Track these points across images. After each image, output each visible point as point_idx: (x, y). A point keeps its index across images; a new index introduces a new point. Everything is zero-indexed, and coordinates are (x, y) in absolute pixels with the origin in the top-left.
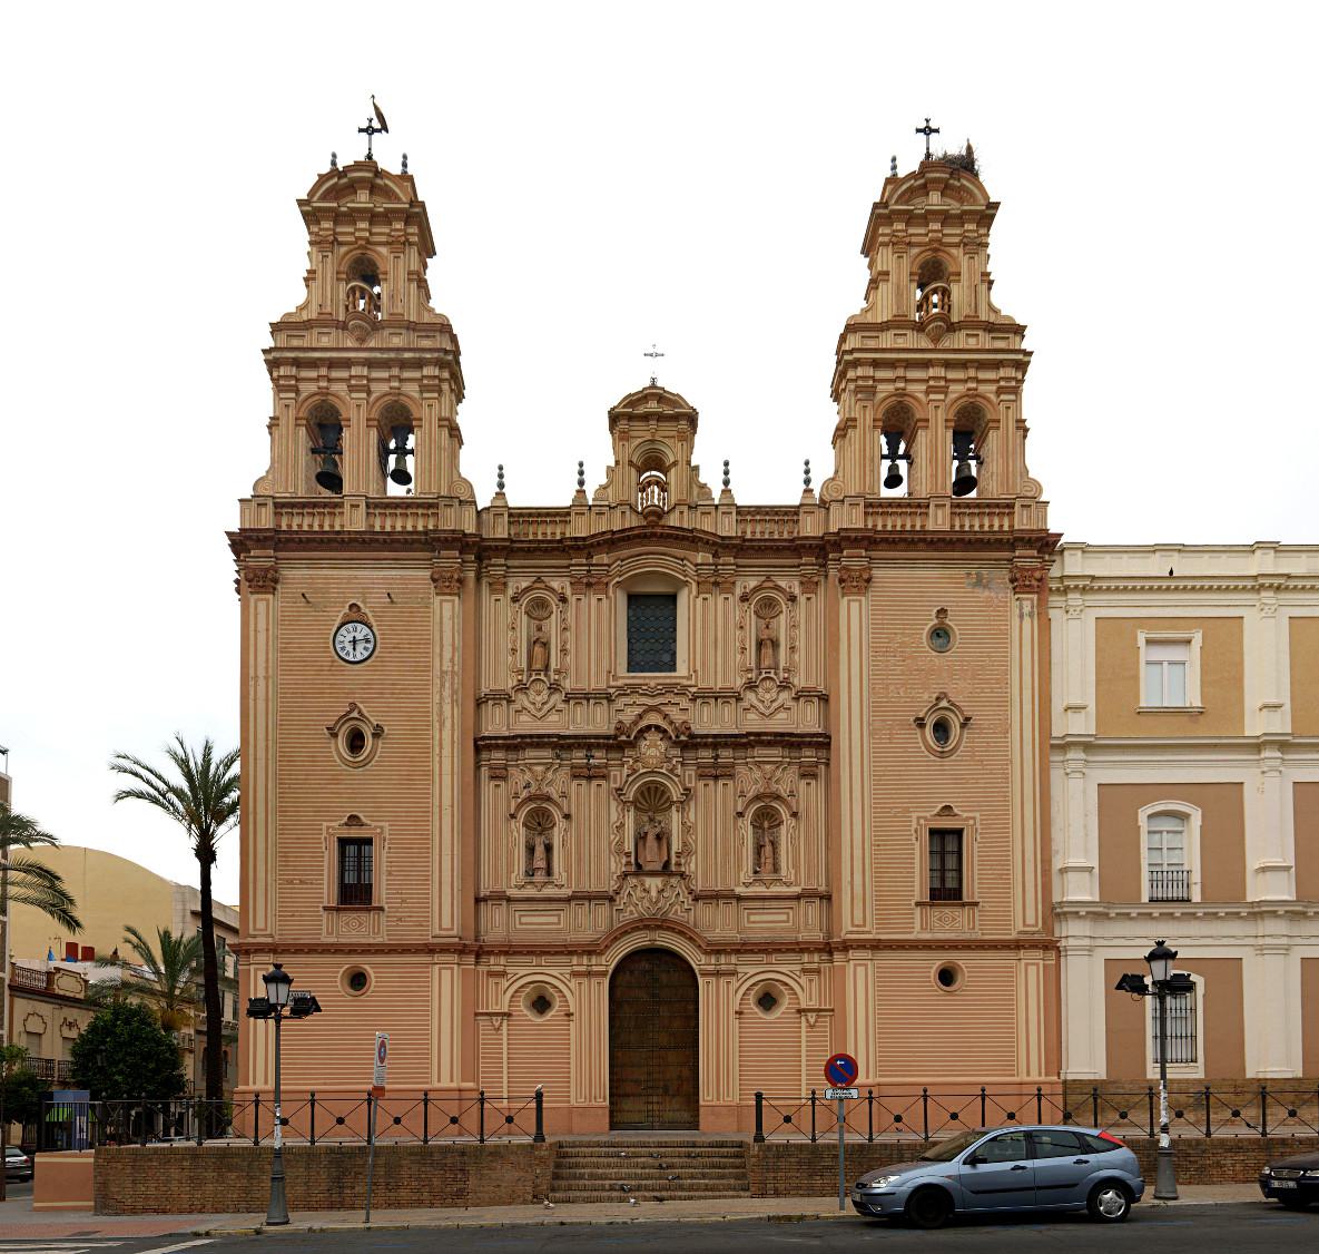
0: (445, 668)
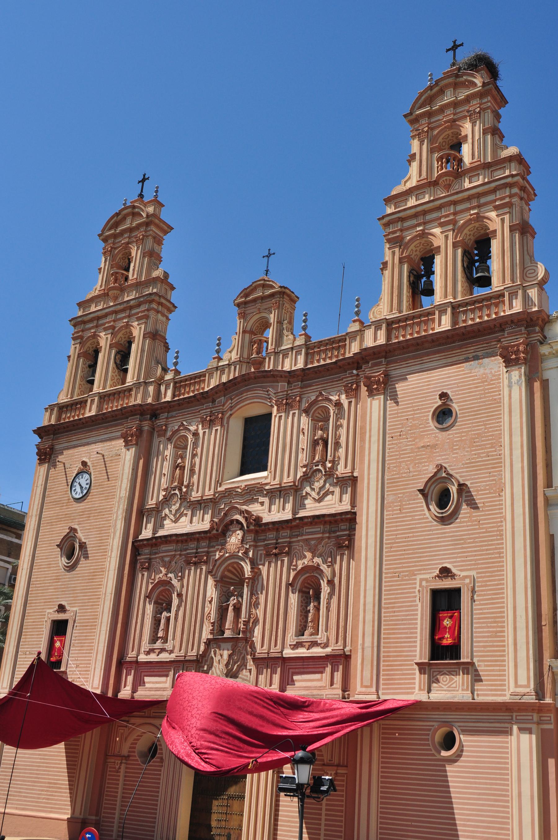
0: (121, 495)
